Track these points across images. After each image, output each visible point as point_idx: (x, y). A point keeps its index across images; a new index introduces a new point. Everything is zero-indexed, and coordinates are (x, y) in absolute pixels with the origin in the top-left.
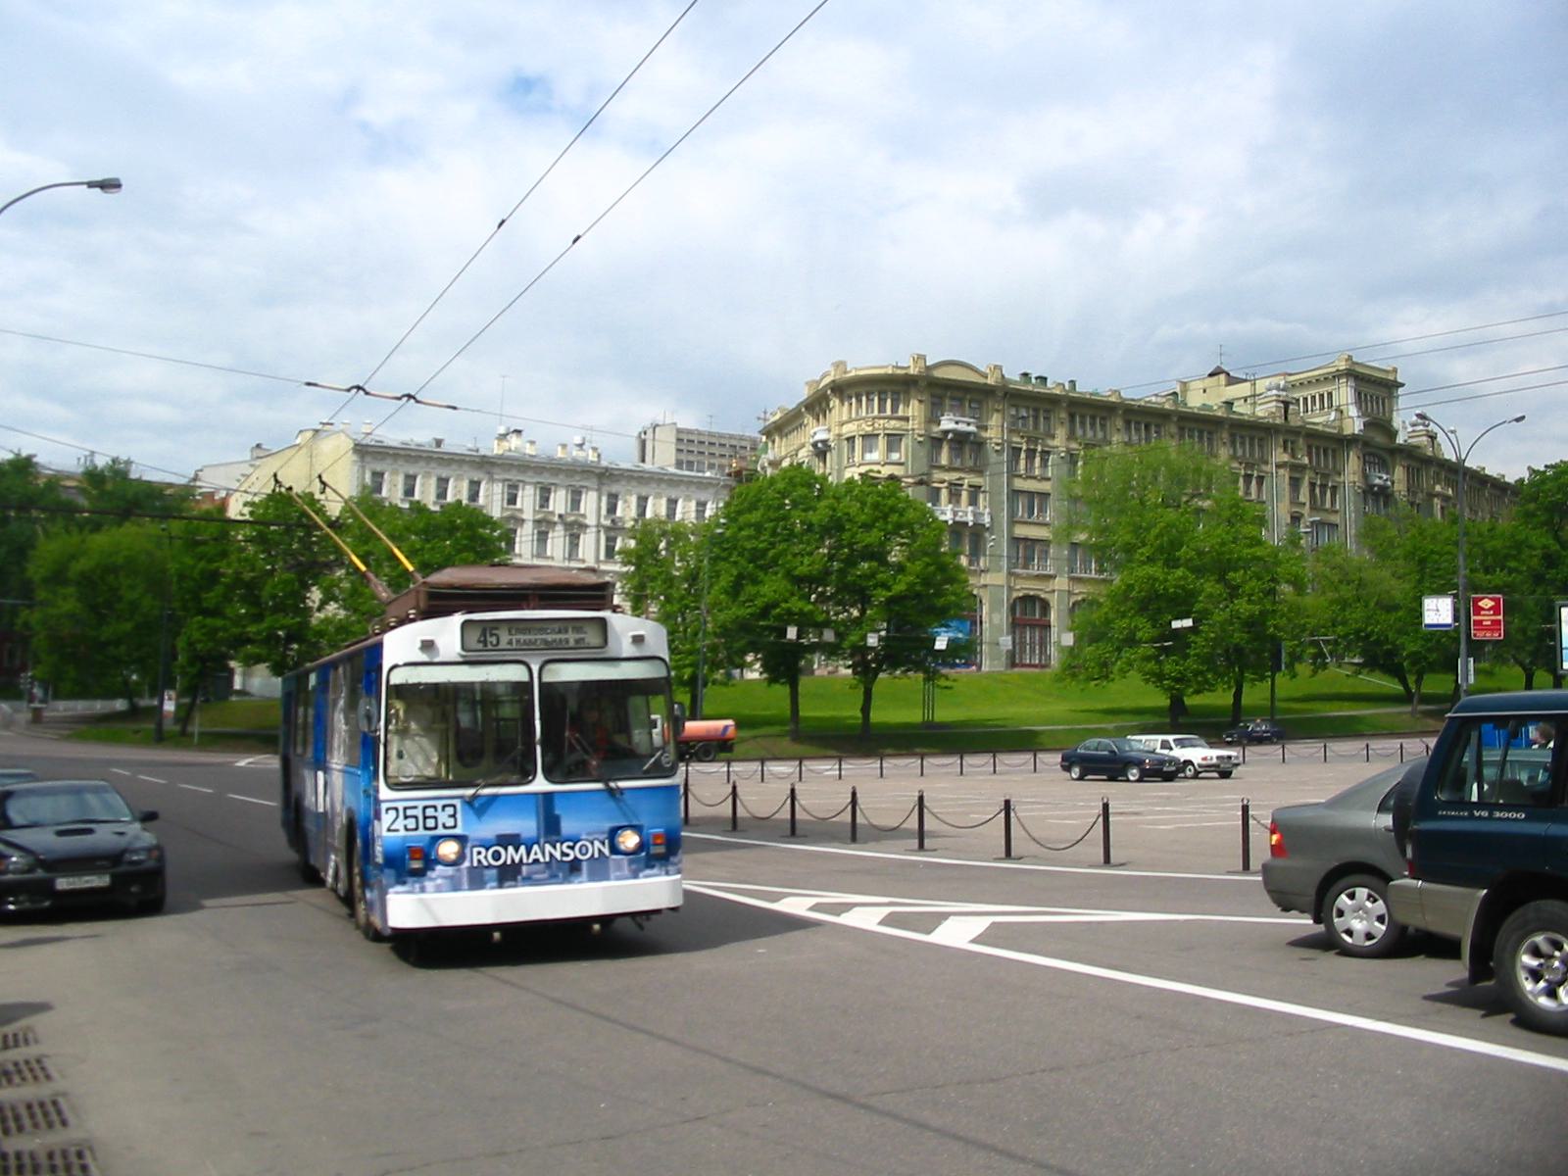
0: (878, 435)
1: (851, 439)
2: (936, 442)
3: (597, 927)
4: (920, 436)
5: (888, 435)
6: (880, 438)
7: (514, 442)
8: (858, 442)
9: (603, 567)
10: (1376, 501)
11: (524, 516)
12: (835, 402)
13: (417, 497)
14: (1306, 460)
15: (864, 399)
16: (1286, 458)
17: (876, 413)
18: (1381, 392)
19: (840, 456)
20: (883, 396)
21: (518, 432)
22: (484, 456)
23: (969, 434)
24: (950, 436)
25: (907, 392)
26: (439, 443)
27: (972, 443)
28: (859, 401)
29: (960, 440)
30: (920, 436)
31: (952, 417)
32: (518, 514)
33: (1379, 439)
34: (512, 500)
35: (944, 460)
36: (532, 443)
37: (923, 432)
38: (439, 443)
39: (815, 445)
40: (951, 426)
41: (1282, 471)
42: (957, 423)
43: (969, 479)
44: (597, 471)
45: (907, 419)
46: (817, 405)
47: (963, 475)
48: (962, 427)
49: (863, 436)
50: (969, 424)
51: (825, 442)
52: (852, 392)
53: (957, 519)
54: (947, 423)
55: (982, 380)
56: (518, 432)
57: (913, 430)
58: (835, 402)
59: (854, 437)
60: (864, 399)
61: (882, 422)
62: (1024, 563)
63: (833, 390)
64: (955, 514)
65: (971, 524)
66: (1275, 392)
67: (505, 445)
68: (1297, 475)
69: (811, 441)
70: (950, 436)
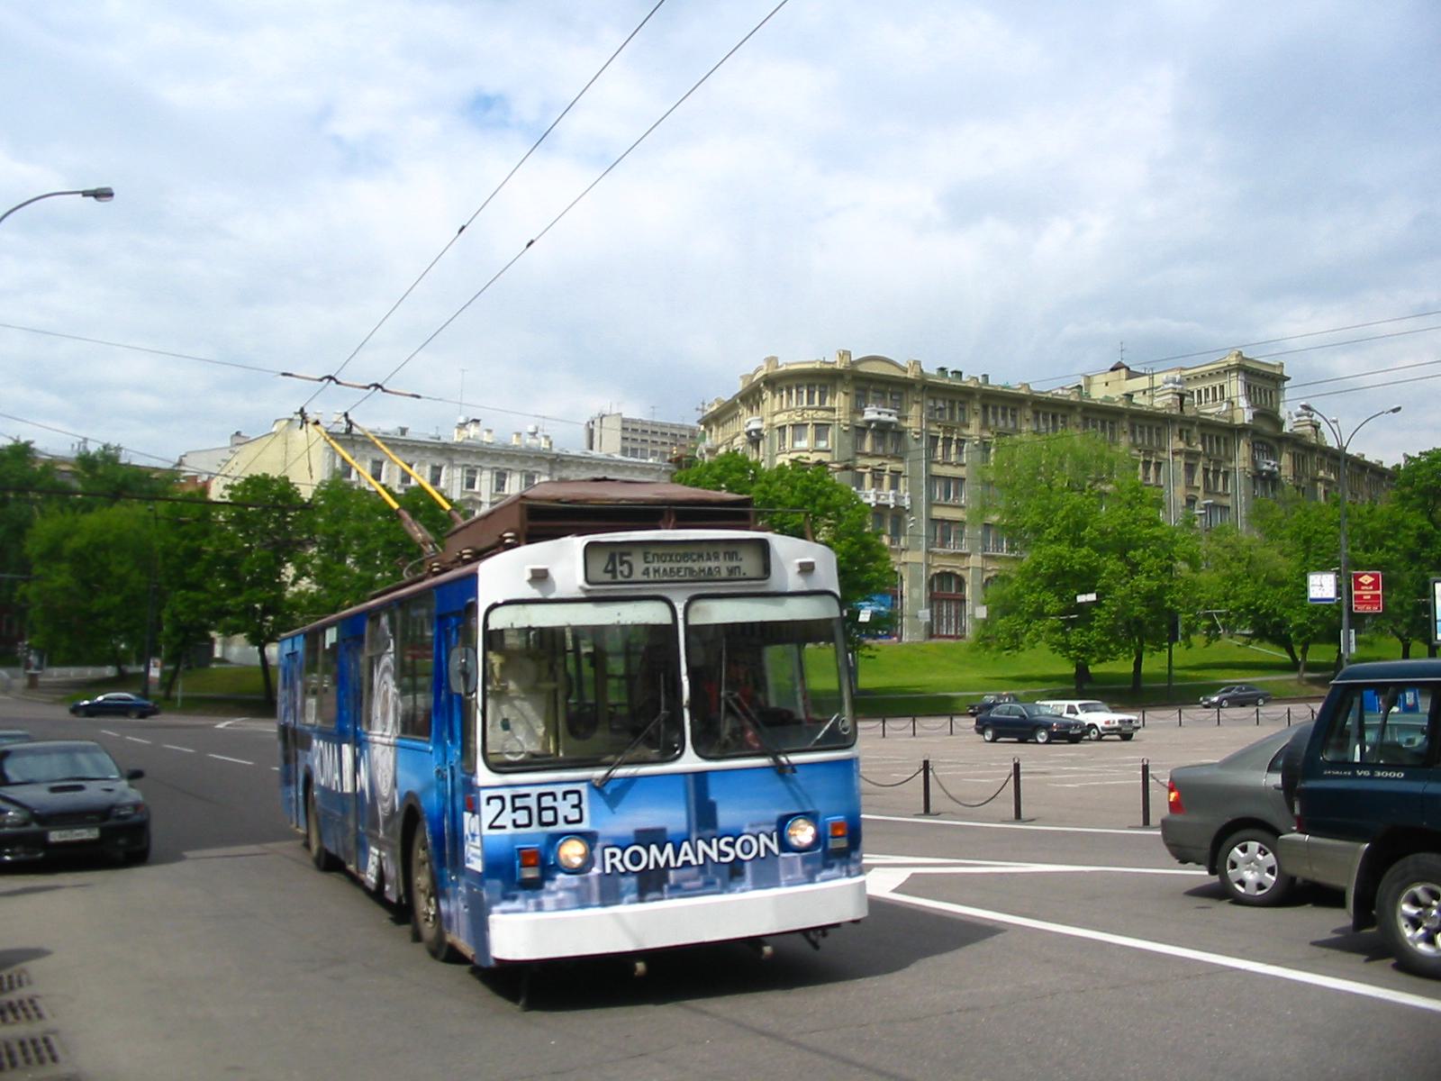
0: (807, 424)
1: (782, 429)
2: (860, 431)
4: (846, 425)
5: (816, 425)
6: (809, 427)
7: (473, 430)
8: (789, 431)
11: (482, 499)
12: (767, 394)
15: (794, 391)
16: (1181, 445)
17: (805, 404)
18: (1270, 386)
19: (772, 444)
20: (800, 390)
21: (476, 421)
22: (445, 444)
24: (873, 425)
25: (834, 386)
26: (403, 431)
27: (893, 432)
28: (790, 394)
29: (882, 429)
30: (846, 425)
31: (874, 408)
32: (476, 497)
33: (1267, 428)
34: (471, 484)
35: (868, 447)
36: (489, 431)
37: (848, 422)
38: (403, 431)
39: (749, 433)
40: (874, 416)
41: (1178, 458)
42: (879, 413)
43: (891, 465)
44: (549, 457)
45: (833, 410)
46: (751, 397)
48: (884, 417)
49: (793, 426)
50: (890, 415)
51: (757, 431)
52: (783, 385)
53: (880, 502)
54: (871, 414)
56: (476, 421)
57: (839, 420)
58: (767, 394)
59: (785, 426)
60: (794, 391)
61: (810, 412)
63: (765, 383)
64: (878, 497)
65: (892, 506)
66: (1171, 385)
67: (464, 433)
68: (1191, 462)
69: (746, 430)
70: (873, 425)
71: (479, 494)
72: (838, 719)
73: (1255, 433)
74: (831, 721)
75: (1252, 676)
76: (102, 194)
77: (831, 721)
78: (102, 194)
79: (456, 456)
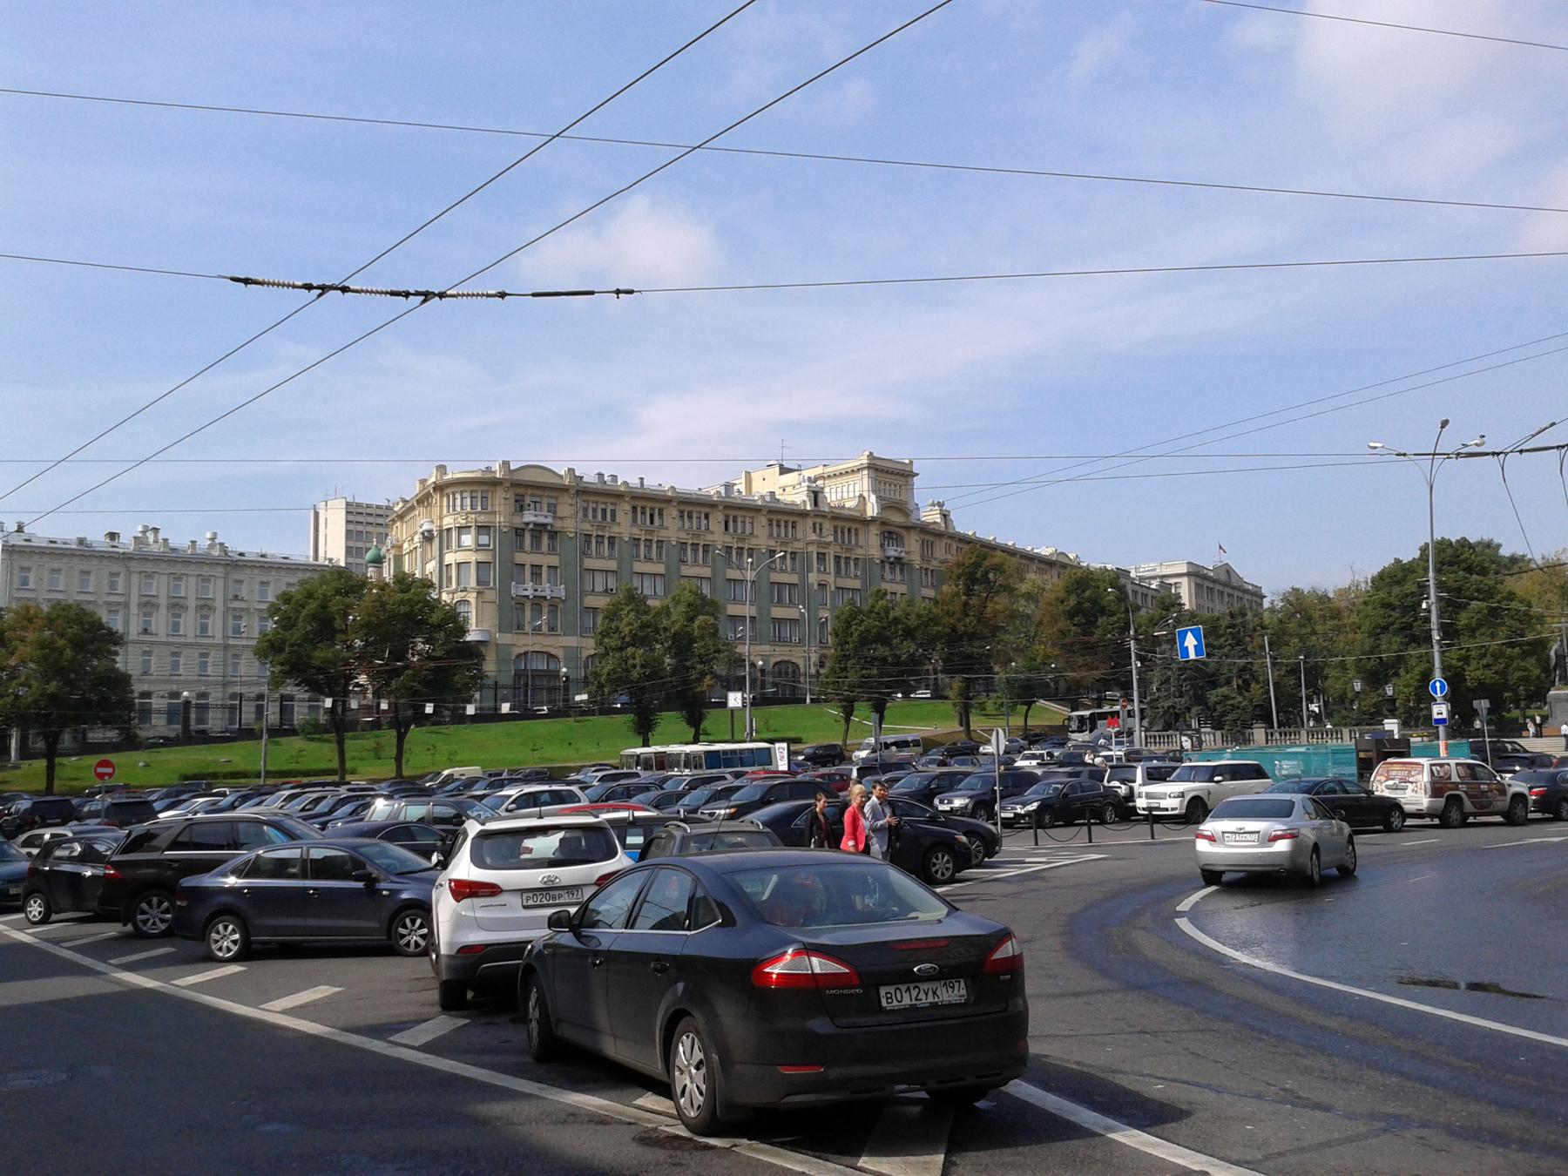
2: (519, 532)
3: (505, 708)
8: (454, 534)
9: (231, 642)
10: (893, 570)
13: (806, 657)
14: (831, 539)
16: (814, 537)
18: (901, 480)
23: (544, 525)
29: (539, 529)
32: (181, 602)
33: (896, 518)
40: (532, 519)
46: (424, 500)
47: (734, 825)
48: (541, 520)
51: (430, 531)
52: (449, 490)
54: (529, 517)
55: (558, 481)
62: (1109, 814)
71: (213, 599)
72: (541, 1001)
73: (883, 523)
74: (1437, 664)
75: (778, 1155)
76: (1445, 424)
77: (1437, 664)
78: (1445, 424)
79: (133, 564)
